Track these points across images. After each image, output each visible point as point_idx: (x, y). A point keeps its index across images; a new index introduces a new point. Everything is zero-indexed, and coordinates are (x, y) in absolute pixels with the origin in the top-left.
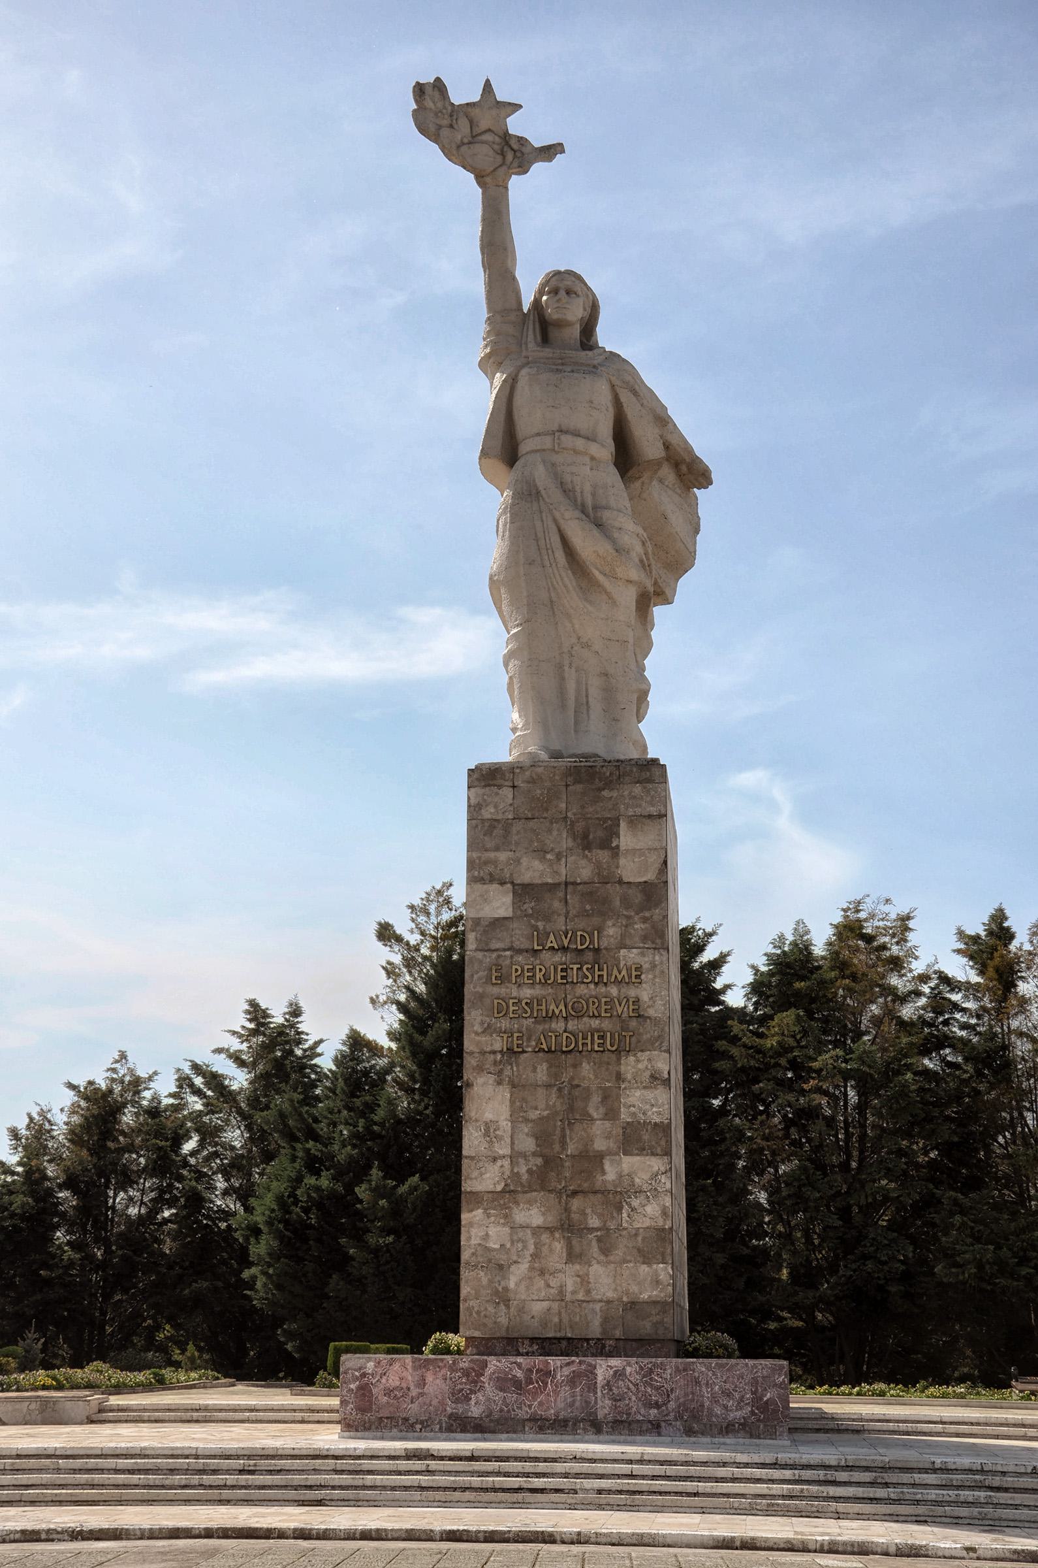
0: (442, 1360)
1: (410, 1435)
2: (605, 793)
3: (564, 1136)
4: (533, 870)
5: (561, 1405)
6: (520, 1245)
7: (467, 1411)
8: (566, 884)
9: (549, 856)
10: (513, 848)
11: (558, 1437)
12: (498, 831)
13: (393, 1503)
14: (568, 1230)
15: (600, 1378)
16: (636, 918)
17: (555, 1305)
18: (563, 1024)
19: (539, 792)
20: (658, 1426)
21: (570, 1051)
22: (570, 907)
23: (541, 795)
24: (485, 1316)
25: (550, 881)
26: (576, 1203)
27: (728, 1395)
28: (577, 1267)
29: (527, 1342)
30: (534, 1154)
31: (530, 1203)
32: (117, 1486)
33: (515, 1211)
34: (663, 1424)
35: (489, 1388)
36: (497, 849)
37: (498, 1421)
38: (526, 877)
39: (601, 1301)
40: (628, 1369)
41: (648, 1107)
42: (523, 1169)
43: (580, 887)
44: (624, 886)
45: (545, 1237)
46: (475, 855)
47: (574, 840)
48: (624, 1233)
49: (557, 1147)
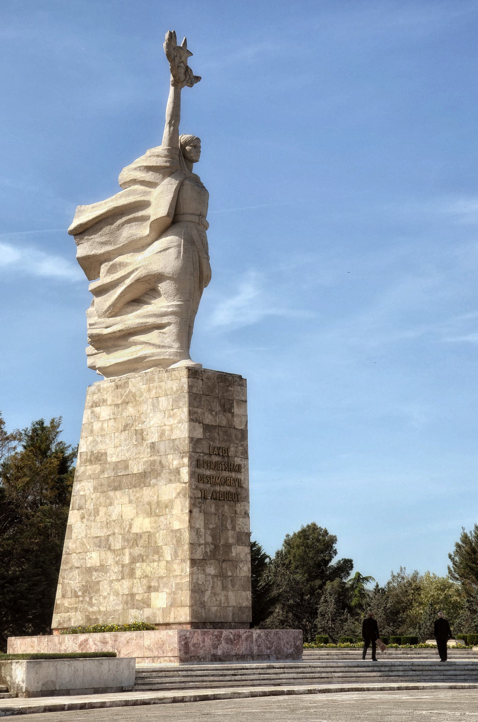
0: (209, 631)
1: (201, 663)
2: (230, 388)
3: (220, 537)
4: (209, 419)
5: (244, 649)
6: (208, 582)
7: (217, 652)
8: (219, 426)
9: (213, 413)
10: (203, 408)
11: (243, 662)
12: (198, 399)
13: (299, 684)
14: (223, 577)
15: (254, 638)
16: (239, 445)
17: (219, 608)
18: (219, 488)
19: (210, 384)
20: (269, 657)
21: (221, 500)
22: (220, 437)
23: (211, 385)
24: (198, 613)
25: (214, 424)
26: (224, 565)
27: (288, 643)
28: (225, 592)
29: (209, 624)
30: (212, 543)
31: (211, 564)
33: (206, 568)
34: (270, 656)
35: (223, 642)
36: (198, 407)
37: (225, 657)
39: (232, 607)
40: (262, 634)
41: (244, 525)
42: (208, 550)
43: (223, 428)
44: (236, 430)
46: (191, 409)
47: (221, 407)
48: (238, 578)
49: (218, 541)
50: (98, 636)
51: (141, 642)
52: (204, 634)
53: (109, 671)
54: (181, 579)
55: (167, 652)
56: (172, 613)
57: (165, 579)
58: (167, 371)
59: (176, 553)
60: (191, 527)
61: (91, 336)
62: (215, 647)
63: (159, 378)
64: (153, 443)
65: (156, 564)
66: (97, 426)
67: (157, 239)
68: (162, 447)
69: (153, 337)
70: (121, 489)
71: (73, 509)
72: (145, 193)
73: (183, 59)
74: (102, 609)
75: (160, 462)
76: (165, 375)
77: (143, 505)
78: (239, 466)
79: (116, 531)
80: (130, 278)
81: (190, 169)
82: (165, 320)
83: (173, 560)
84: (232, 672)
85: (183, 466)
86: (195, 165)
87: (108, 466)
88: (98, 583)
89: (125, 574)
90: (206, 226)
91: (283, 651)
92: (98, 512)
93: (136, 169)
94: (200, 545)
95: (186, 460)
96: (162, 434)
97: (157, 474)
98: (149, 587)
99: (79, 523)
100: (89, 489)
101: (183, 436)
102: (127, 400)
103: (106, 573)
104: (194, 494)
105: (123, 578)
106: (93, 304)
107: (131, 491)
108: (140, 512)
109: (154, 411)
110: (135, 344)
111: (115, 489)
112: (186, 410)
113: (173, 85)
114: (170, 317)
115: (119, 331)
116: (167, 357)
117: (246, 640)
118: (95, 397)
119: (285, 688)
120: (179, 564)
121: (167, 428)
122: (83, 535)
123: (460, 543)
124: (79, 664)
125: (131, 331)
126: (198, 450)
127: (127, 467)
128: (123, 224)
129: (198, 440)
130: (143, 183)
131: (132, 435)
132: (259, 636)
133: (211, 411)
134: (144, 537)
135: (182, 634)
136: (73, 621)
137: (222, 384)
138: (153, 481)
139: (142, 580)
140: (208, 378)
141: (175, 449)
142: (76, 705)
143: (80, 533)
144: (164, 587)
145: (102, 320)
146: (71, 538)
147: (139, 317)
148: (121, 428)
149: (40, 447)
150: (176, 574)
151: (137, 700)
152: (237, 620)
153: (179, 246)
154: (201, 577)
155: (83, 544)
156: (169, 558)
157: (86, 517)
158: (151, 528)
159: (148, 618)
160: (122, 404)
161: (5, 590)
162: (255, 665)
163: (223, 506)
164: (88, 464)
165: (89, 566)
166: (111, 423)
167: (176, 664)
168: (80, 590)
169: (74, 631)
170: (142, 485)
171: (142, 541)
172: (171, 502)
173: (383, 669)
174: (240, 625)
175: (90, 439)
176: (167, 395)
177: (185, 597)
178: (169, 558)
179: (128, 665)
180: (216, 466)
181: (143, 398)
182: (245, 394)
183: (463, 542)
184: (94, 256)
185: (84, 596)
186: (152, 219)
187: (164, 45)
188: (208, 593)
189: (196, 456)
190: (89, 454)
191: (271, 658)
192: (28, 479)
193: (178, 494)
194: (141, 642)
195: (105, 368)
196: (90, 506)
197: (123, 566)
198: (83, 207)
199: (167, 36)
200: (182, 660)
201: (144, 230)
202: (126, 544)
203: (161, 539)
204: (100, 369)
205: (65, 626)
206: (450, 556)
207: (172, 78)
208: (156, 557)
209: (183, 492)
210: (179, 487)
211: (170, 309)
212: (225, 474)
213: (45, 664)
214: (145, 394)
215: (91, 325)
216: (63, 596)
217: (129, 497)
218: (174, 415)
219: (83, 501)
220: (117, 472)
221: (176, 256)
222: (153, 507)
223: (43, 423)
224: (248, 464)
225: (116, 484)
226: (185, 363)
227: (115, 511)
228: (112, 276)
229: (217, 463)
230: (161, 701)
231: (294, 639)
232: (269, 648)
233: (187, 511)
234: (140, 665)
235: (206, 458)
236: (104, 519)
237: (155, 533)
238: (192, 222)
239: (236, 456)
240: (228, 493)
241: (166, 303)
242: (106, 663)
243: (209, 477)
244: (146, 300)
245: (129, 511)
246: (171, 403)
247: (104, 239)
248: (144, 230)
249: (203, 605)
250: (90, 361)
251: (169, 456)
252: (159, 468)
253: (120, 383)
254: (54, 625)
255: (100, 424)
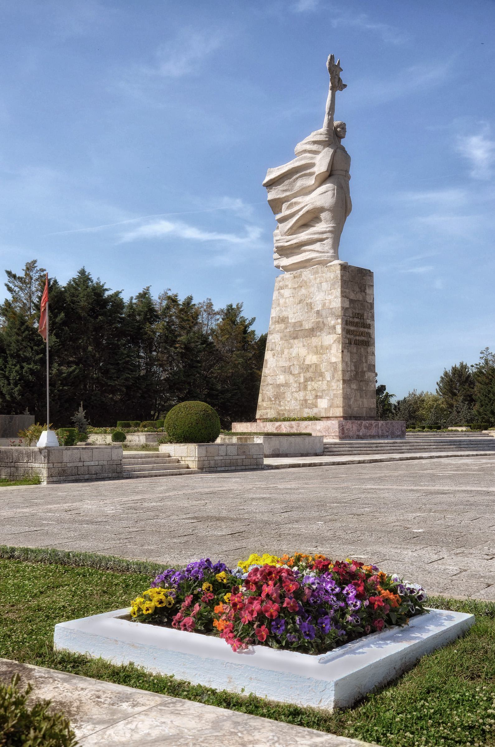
2: (364, 277)
4: (352, 296)
9: (355, 292)
12: (346, 284)
31: (354, 383)
32: (365, 451)
37: (364, 436)
38: (351, 297)
45: (356, 392)
50: (287, 423)
51: (314, 427)
52: (352, 423)
53: (309, 443)
54: (336, 391)
55: (331, 433)
56: (331, 411)
57: (326, 392)
58: (326, 267)
59: (333, 377)
60: (343, 360)
61: (277, 247)
62: (358, 430)
63: (322, 271)
64: (318, 310)
65: (320, 382)
66: (282, 301)
67: (320, 185)
68: (324, 313)
69: (317, 246)
70: (298, 338)
71: (268, 350)
72: (312, 158)
73: (337, 72)
74: (287, 408)
75: (323, 322)
76: (326, 269)
77: (312, 348)
78: (369, 325)
79: (295, 363)
80: (302, 211)
81: (340, 142)
82: (325, 236)
83: (331, 380)
84: (375, 445)
85: (338, 324)
86: (342, 140)
87: (289, 324)
88: (284, 393)
89: (301, 388)
90: (349, 178)
91: (395, 433)
92: (283, 352)
93: (306, 143)
94: (348, 371)
95: (340, 321)
96: (324, 305)
97: (321, 329)
98: (317, 396)
99: (272, 359)
100: (277, 339)
101: (338, 306)
102: (301, 285)
103: (289, 387)
104: (344, 341)
105: (300, 390)
106: (278, 228)
107: (304, 339)
108: (310, 352)
109: (319, 291)
110: (305, 251)
111: (294, 338)
112: (339, 290)
113: (331, 89)
114: (328, 234)
115: (295, 244)
116: (326, 259)
117: (375, 427)
118: (281, 283)
119: (418, 455)
120: (335, 382)
121: (327, 301)
122: (274, 365)
123: (443, 376)
124: (292, 439)
125: (303, 243)
126: (347, 315)
127: (301, 325)
128: (297, 178)
129: (347, 309)
130: (310, 152)
131: (304, 306)
132: (382, 425)
133: (353, 291)
134: (312, 367)
135: (340, 423)
136: (269, 414)
137: (359, 275)
138: (318, 333)
139: (312, 392)
140: (352, 271)
141: (332, 314)
142: (307, 464)
143: (272, 364)
144: (326, 396)
145: (284, 237)
146: (267, 367)
147: (308, 234)
148: (297, 301)
149: (231, 319)
150: (334, 388)
151: (339, 462)
152: (368, 416)
153: (334, 190)
154: (349, 390)
155: (274, 371)
156: (329, 379)
157: (276, 355)
158: (317, 361)
159: (316, 414)
160: (298, 287)
161: (219, 397)
162: (387, 441)
163: (361, 349)
164: (277, 323)
165: (278, 383)
166: (291, 299)
167: (337, 441)
168: (273, 397)
169: (271, 420)
170: (311, 336)
171: (312, 369)
172: (330, 346)
173: (455, 443)
174: (369, 418)
175: (278, 309)
176: (327, 281)
177: (339, 401)
178: (329, 379)
179: (320, 440)
180: (356, 325)
181: (311, 283)
182: (372, 281)
183: (445, 375)
184: (279, 199)
185: (275, 401)
186: (317, 173)
187: (327, 63)
188: (352, 400)
189: (345, 319)
190: (277, 318)
191: (389, 437)
192: (228, 336)
193: (335, 341)
194: (314, 427)
195: (286, 266)
196: (278, 348)
197: (300, 384)
198: (272, 169)
199: (329, 57)
200: (341, 438)
201: (311, 181)
202: (301, 371)
203: (323, 368)
204: (282, 267)
205: (265, 417)
206: (437, 383)
207: (330, 85)
208: (320, 378)
209: (338, 340)
210: (335, 337)
211: (328, 229)
212: (362, 329)
213: (274, 438)
214: (312, 281)
215: (277, 241)
216: (263, 401)
217: (303, 343)
218: (332, 293)
219: (274, 345)
220: (295, 328)
221: (332, 196)
222: (319, 349)
223: (232, 306)
224: (374, 324)
225: (295, 335)
226: (336, 262)
227: (294, 352)
228: (290, 210)
229: (357, 323)
230: (352, 462)
231: (401, 426)
232: (388, 432)
233: (341, 351)
234: (325, 440)
235: (351, 319)
236: (287, 356)
237: (319, 365)
238: (341, 175)
239: (368, 319)
240: (363, 341)
241: (326, 226)
242: (307, 439)
243: (352, 331)
244: (312, 224)
245: (303, 352)
246: (329, 286)
247: (285, 188)
248: (311, 181)
249: (350, 406)
250: (276, 263)
251: (328, 318)
252: (322, 326)
253: (296, 275)
254: (257, 416)
255: (284, 300)
